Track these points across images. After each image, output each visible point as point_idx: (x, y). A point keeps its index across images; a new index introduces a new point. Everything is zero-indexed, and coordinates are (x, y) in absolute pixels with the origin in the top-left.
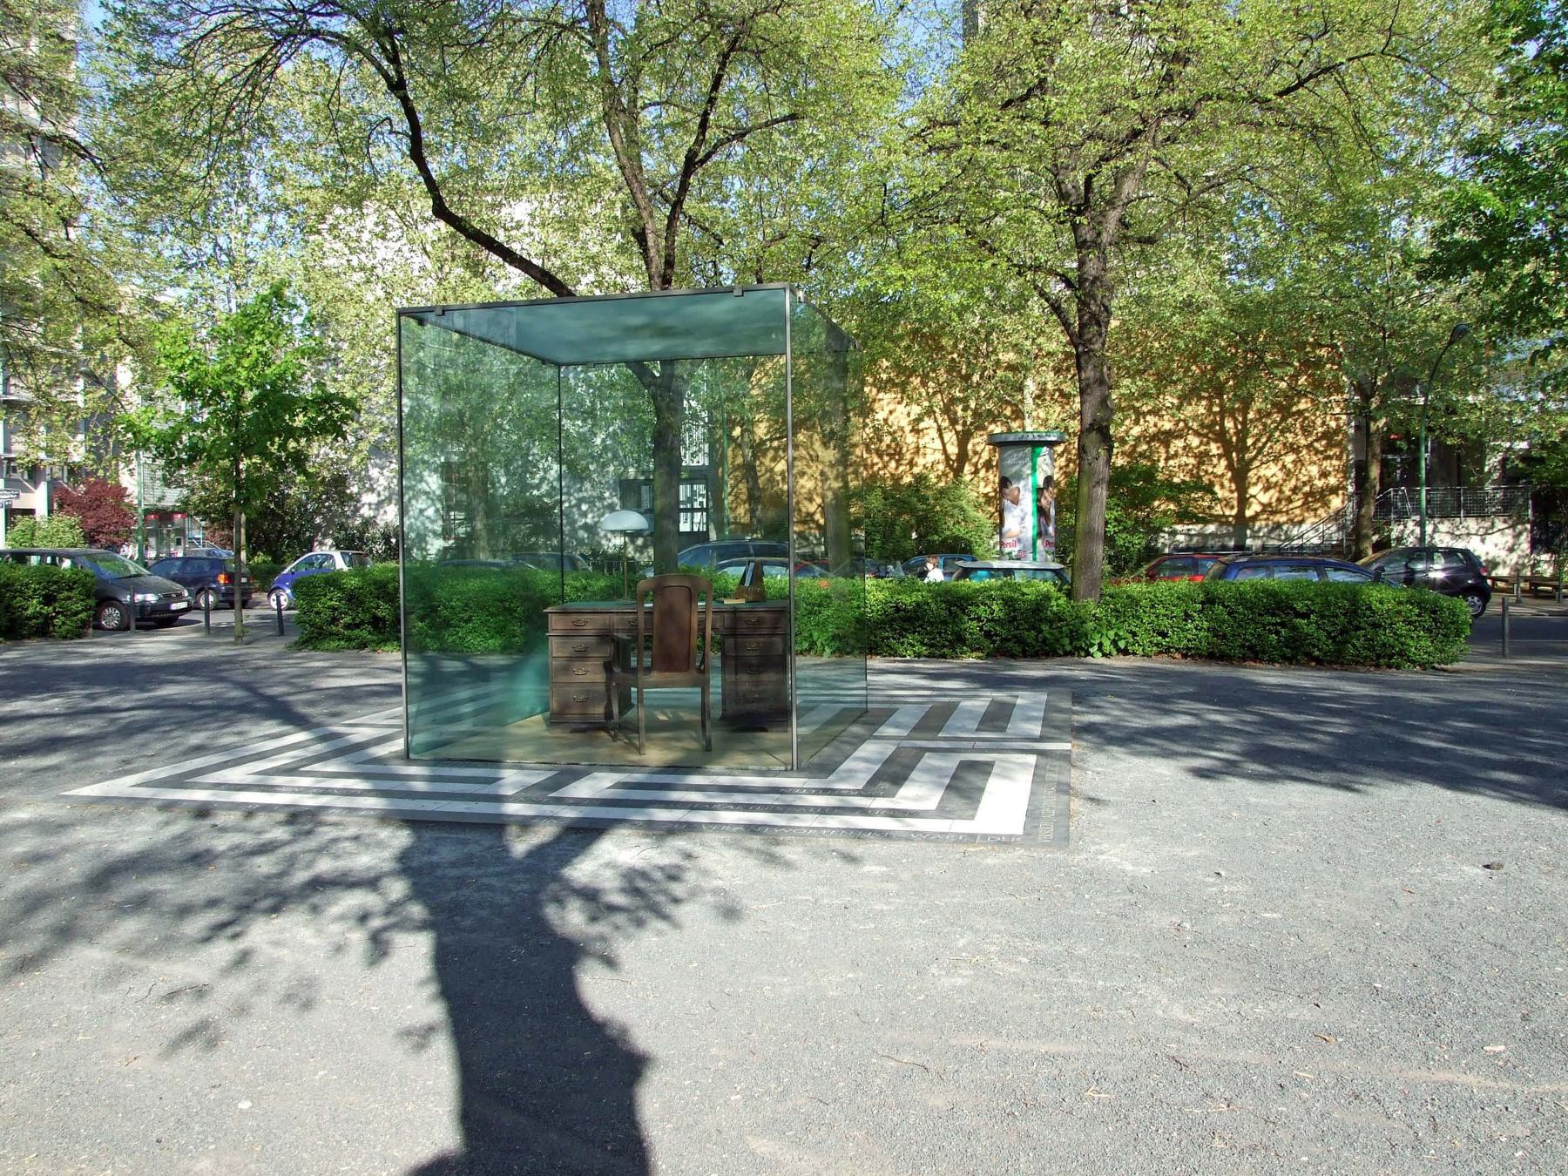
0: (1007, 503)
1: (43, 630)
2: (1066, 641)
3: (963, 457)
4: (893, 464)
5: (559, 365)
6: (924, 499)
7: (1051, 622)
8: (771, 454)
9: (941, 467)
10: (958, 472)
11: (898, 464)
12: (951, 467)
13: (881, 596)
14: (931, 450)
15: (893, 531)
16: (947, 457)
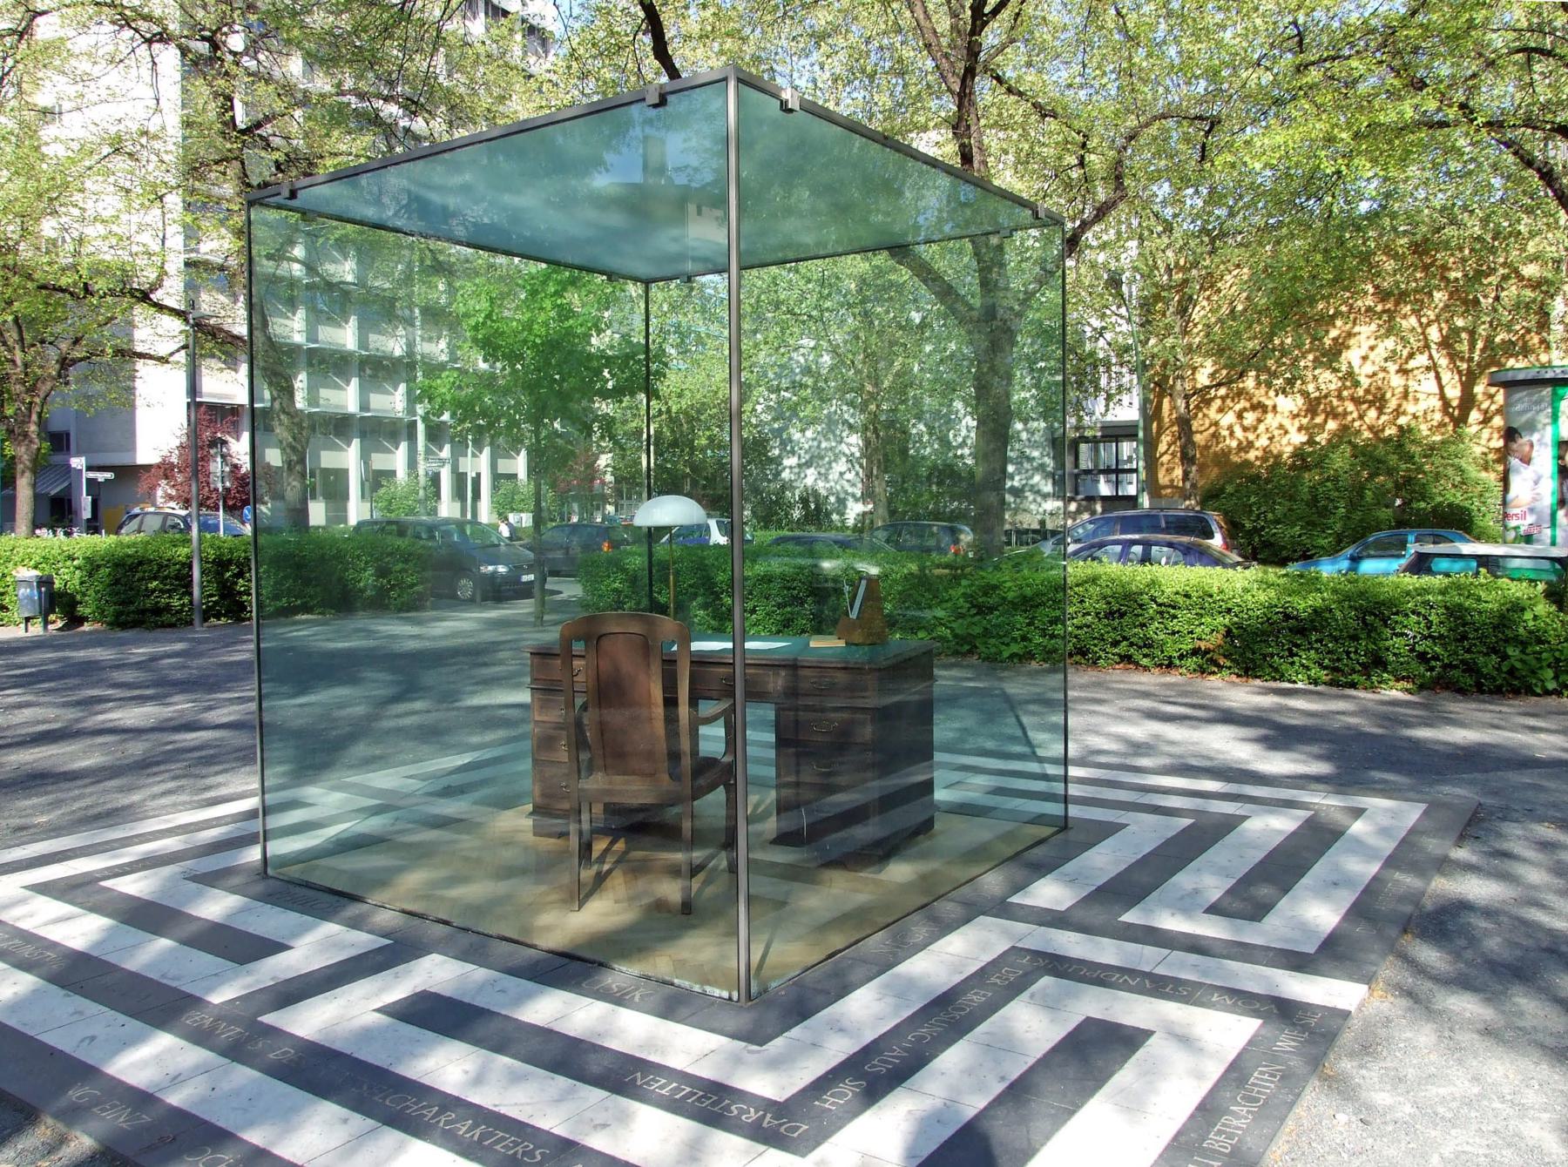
0: (1514, 462)
1: (380, 603)
2: (1550, 673)
3: (1468, 401)
4: (1372, 413)
5: (647, 283)
6: (1410, 458)
7: (1523, 644)
8: (1217, 403)
9: (1438, 416)
10: (1460, 420)
11: (1381, 411)
12: (1451, 416)
13: (1262, 597)
14: (1423, 398)
15: (1362, 497)
16: (1446, 404)
